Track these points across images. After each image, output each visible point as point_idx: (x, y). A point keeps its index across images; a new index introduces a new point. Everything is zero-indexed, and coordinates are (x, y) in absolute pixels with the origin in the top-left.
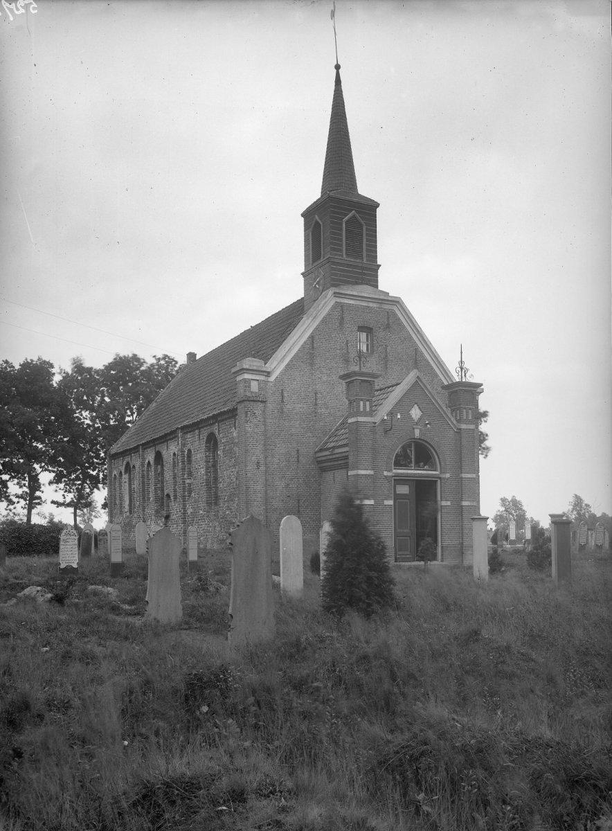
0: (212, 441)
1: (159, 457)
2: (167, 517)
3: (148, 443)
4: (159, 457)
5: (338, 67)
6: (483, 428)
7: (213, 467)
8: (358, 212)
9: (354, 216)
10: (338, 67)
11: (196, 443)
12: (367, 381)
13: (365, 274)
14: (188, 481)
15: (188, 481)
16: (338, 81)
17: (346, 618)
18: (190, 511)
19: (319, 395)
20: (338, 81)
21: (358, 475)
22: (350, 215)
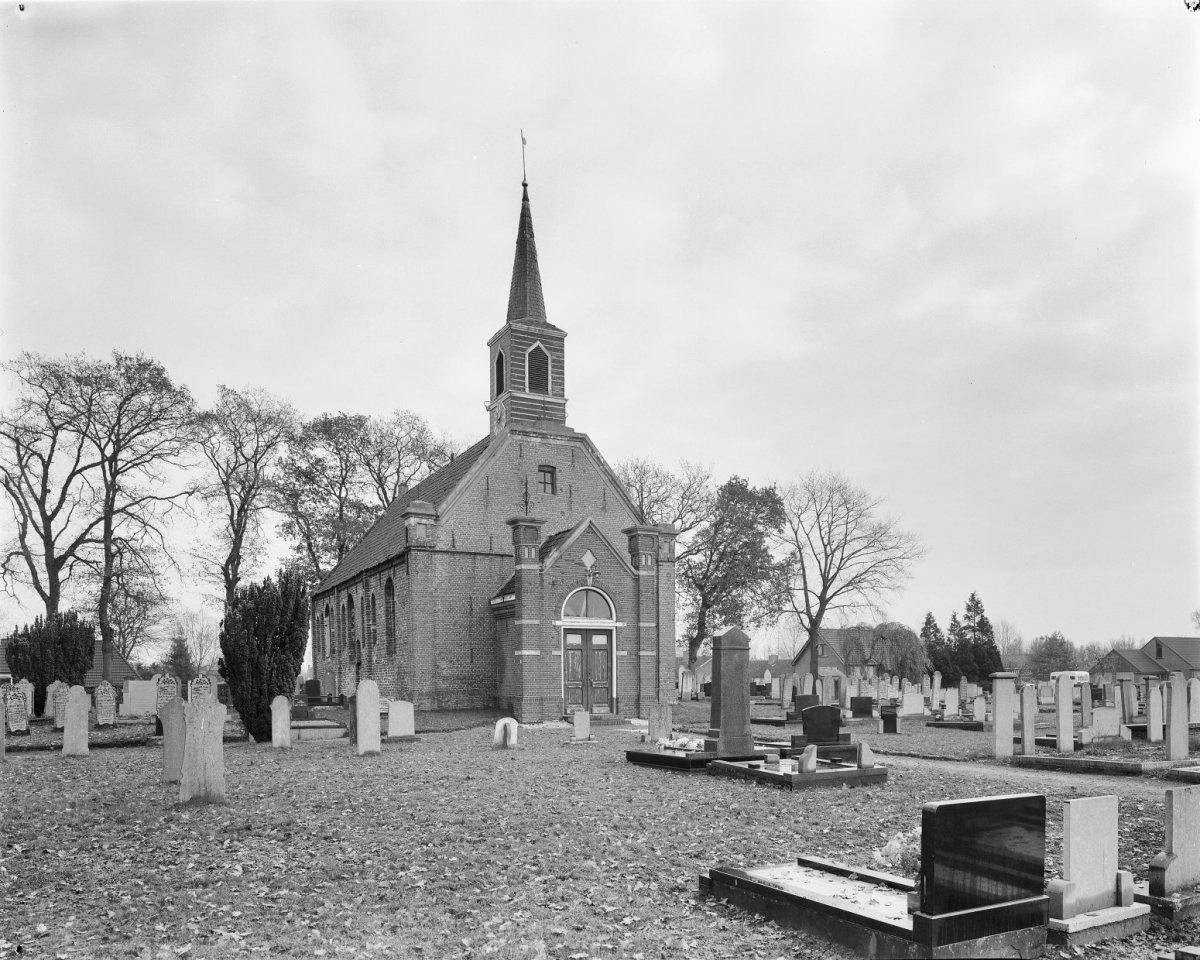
0: (389, 588)
1: (350, 598)
2: (359, 664)
3: (342, 584)
4: (350, 598)
5: (525, 185)
6: (165, 375)
7: (390, 613)
8: (541, 341)
9: (538, 348)
10: (525, 185)
11: (376, 585)
12: (532, 527)
13: (542, 408)
14: (372, 627)
15: (372, 627)
16: (525, 198)
17: (767, 655)
18: (374, 659)
19: (495, 540)
20: (525, 198)
21: (323, 628)
22: (535, 346)
